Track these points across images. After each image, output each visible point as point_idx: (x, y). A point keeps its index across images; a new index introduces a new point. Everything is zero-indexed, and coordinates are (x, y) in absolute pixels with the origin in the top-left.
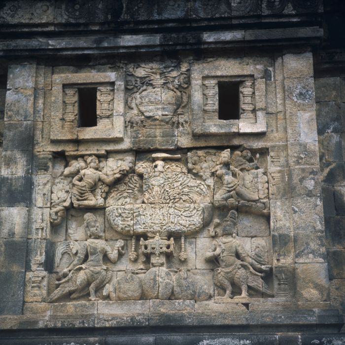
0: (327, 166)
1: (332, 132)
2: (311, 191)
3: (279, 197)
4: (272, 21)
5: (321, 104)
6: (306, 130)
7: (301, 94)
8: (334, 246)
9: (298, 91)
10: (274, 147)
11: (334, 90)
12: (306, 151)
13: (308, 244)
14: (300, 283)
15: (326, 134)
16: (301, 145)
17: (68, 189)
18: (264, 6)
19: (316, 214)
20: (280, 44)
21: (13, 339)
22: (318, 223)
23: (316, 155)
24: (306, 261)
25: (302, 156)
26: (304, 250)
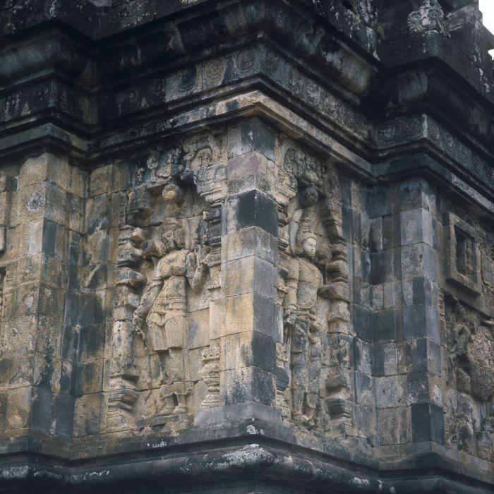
0: (92, 270)
1: (100, 229)
2: (29, 309)
3: (7, 319)
4: (14, 126)
5: (94, 199)
6: (34, 242)
7: (35, 202)
8: (88, 358)
9: (32, 199)
10: (9, 265)
11: (106, 180)
12: (31, 265)
13: (20, 368)
14: (9, 411)
15: (95, 233)
16: (27, 259)
17: (351, 243)
18: (6, 111)
19: (31, 333)
20: (19, 150)
21: (142, 461)
22: (30, 344)
23: (37, 269)
24: (17, 386)
25: (27, 272)
26: (17, 374)
